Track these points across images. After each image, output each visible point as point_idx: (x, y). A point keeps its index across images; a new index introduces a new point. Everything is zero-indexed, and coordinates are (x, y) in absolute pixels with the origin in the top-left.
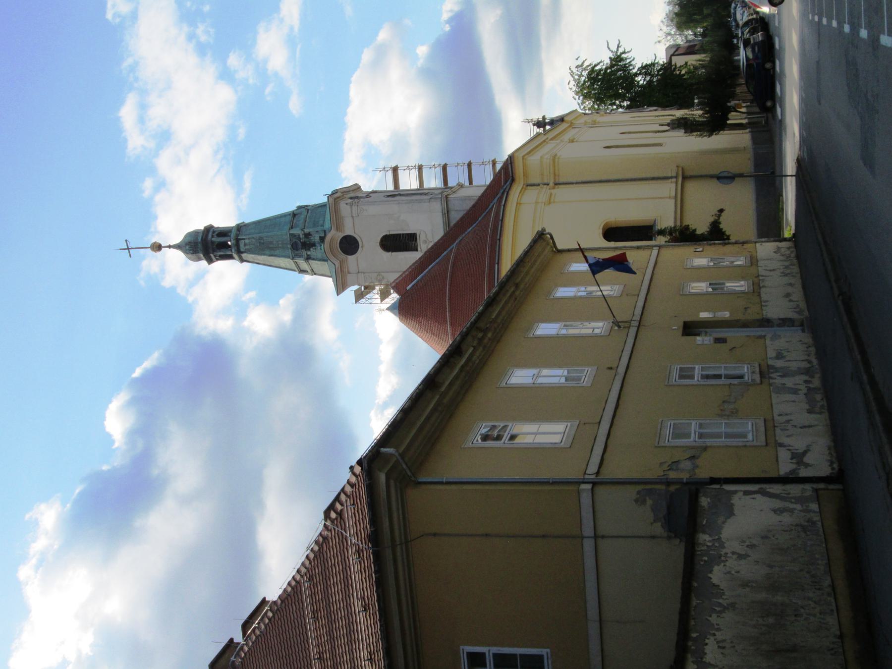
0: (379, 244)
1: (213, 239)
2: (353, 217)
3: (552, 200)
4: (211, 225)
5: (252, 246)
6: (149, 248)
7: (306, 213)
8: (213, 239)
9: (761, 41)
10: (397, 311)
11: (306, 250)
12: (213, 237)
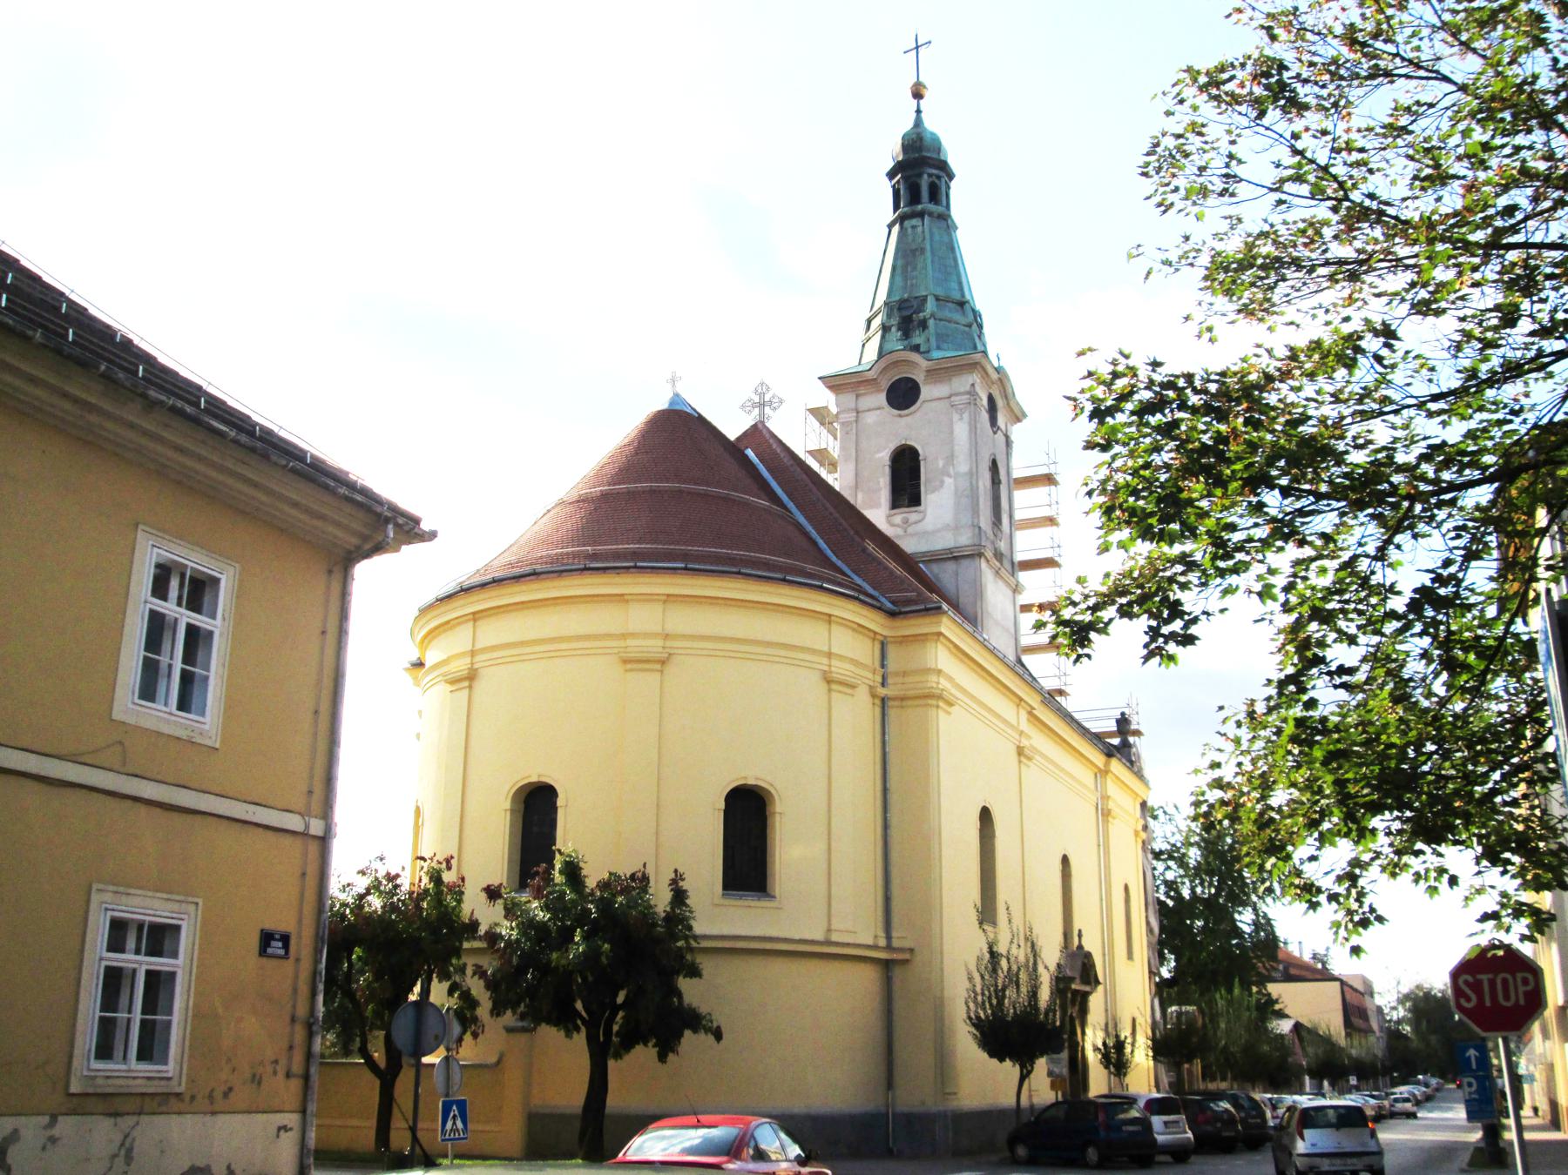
1: (925, 176)
3: (834, 687)
5: (910, 238)
9: (1155, 1140)
12: (930, 175)
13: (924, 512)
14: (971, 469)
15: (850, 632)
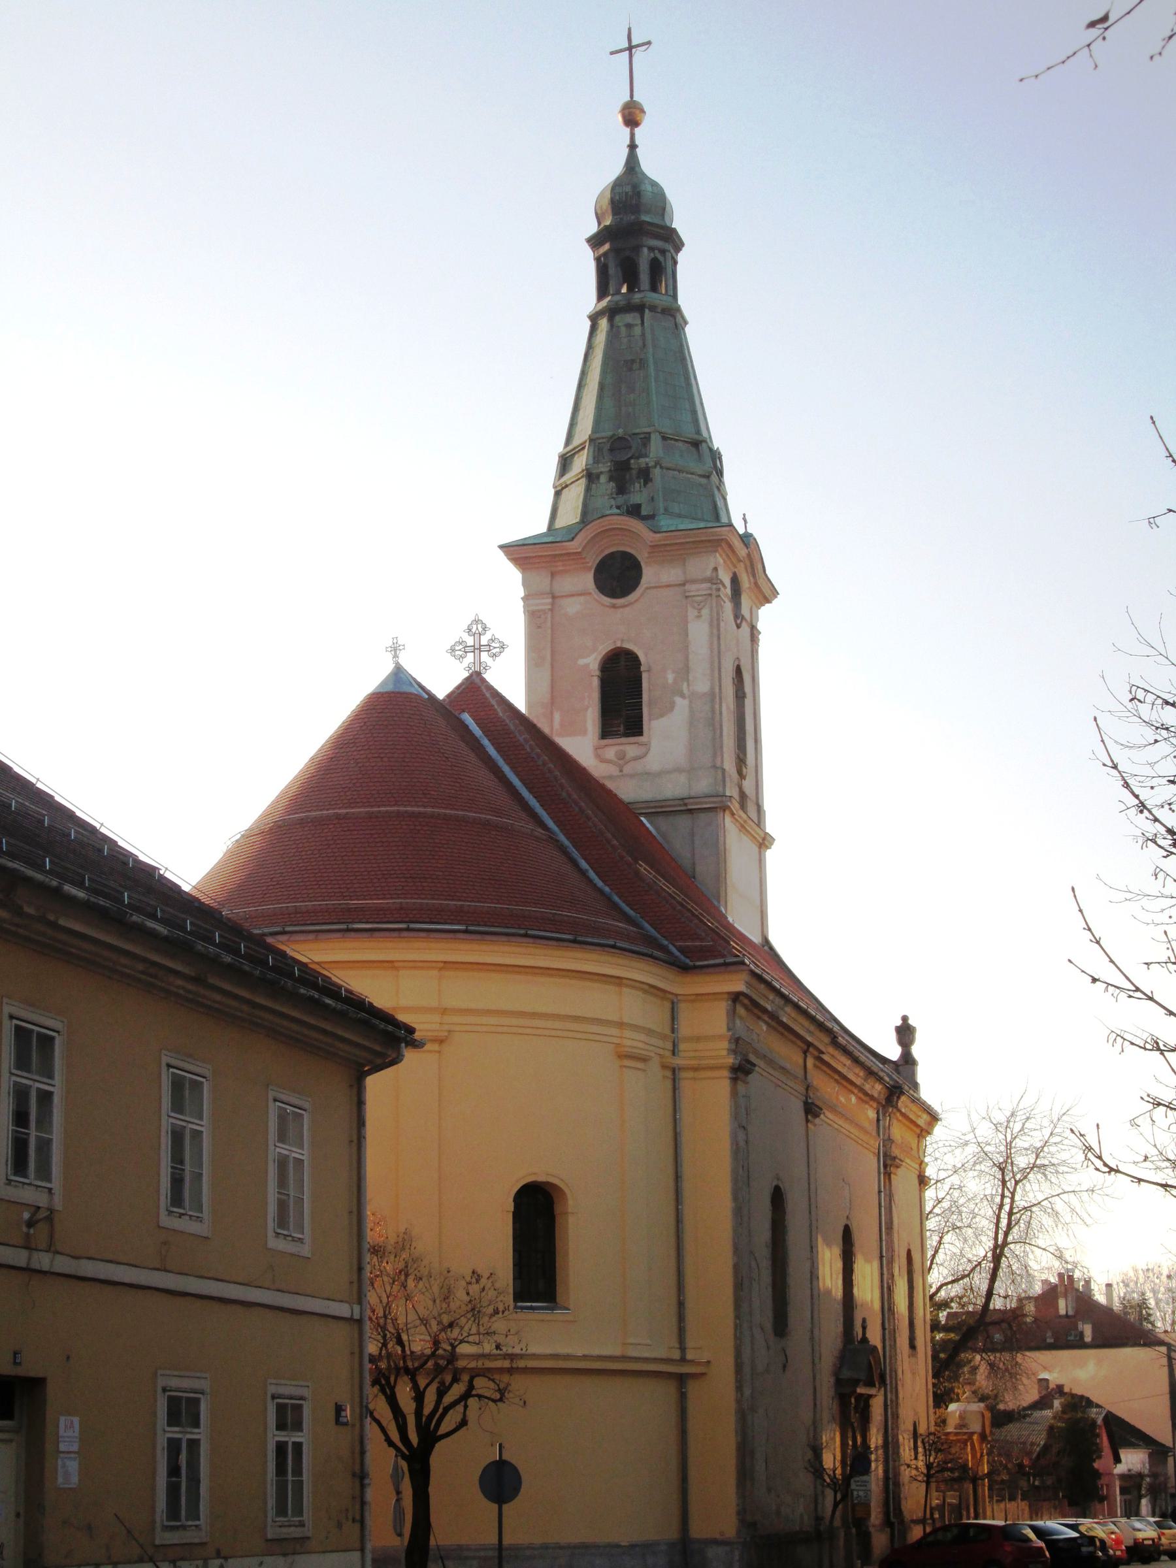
0: (619, 644)
1: (645, 250)
2: (684, 585)
4: (683, 245)
6: (632, 96)
7: (700, 473)
8: (645, 250)
10: (390, 688)
11: (610, 470)
12: (651, 249)
13: (647, 745)
14: (712, 688)
15: (640, 993)
